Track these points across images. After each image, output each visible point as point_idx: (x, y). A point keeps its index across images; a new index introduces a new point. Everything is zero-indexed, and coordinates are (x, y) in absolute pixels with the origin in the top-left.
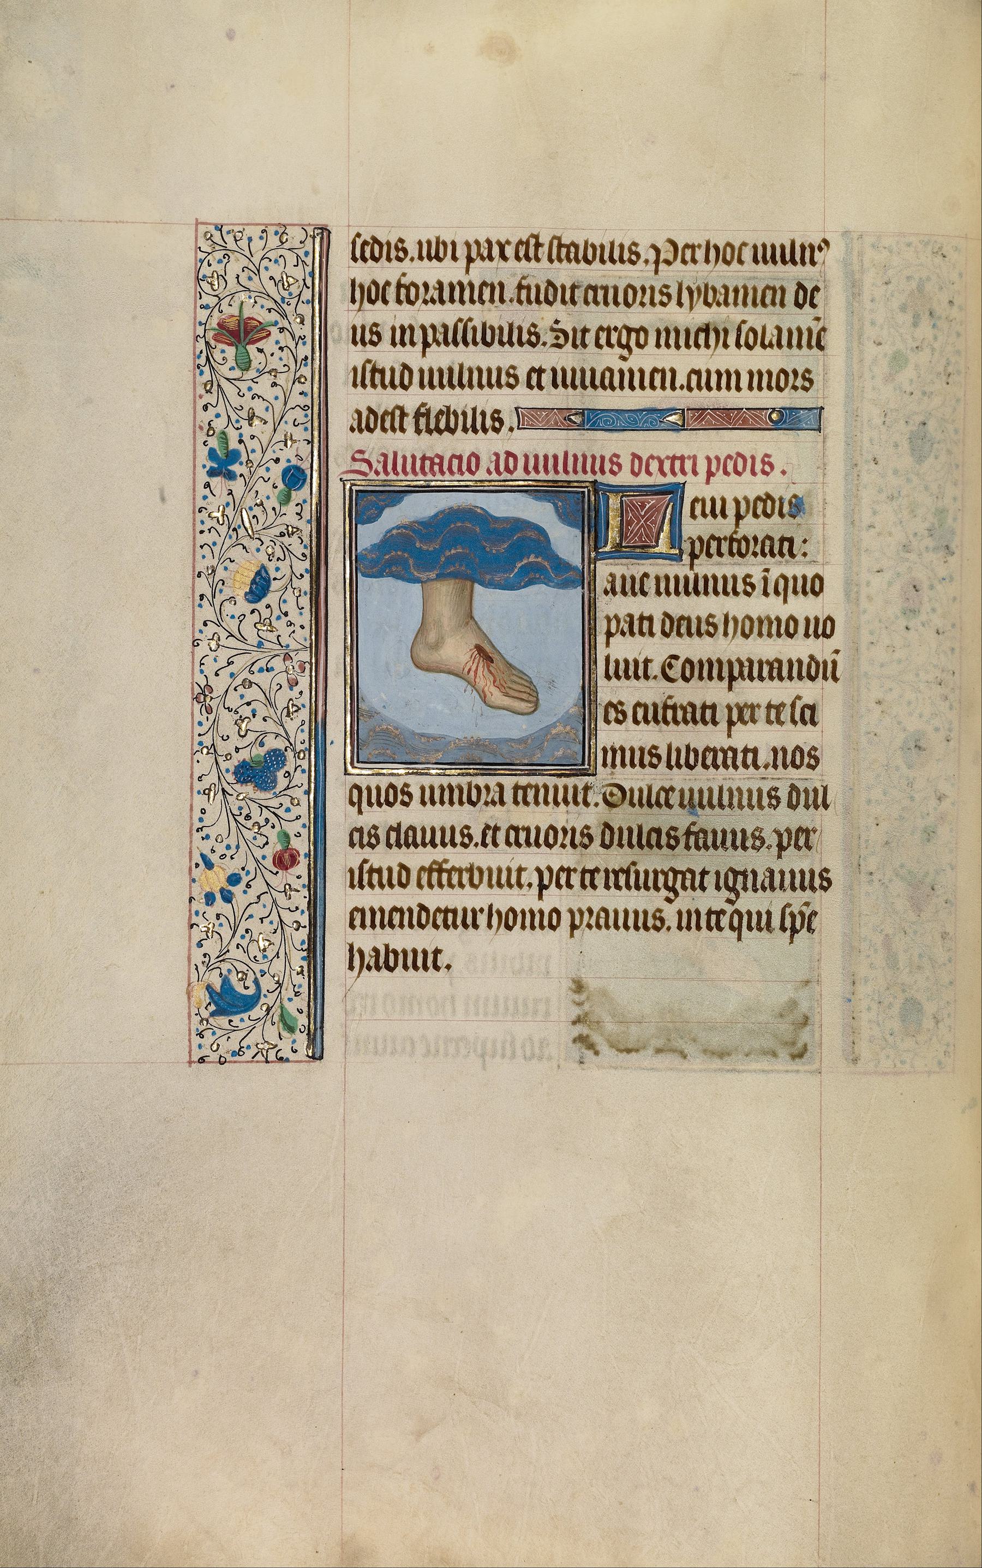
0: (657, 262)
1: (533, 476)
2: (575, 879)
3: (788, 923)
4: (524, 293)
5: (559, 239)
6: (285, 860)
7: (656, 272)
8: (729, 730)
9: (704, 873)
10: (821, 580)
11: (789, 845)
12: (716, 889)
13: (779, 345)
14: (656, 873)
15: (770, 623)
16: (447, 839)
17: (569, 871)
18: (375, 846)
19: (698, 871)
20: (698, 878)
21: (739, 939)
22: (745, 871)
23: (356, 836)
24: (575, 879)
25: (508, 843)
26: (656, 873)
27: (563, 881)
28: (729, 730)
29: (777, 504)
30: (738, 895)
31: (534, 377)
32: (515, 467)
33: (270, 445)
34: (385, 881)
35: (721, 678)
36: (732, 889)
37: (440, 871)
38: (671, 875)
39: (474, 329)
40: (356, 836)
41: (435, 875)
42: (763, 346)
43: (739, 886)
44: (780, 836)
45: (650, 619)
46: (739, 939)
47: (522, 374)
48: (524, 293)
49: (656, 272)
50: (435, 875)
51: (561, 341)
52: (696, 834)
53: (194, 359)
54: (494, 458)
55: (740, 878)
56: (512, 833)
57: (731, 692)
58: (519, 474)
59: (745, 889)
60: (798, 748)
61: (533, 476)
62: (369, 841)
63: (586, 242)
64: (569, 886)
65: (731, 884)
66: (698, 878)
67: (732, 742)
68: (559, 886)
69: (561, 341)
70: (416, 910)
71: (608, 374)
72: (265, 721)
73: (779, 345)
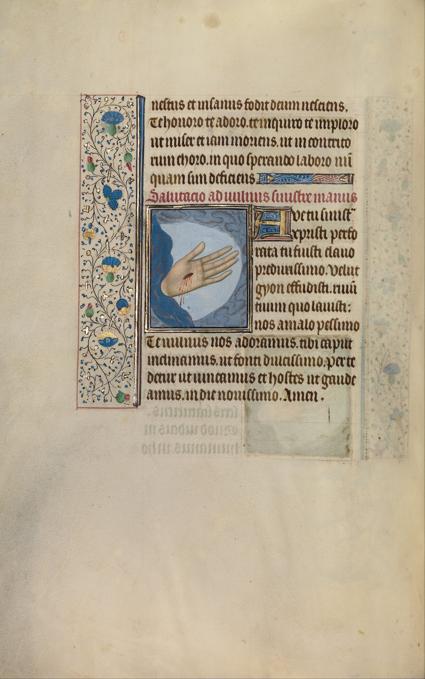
1: (228, 202)
2: (345, 362)
9: (214, 392)
10: (353, 250)
15: (325, 122)
16: (197, 344)
17: (341, 359)
24: (345, 362)
27: (339, 363)
30: (327, 386)
31: (200, 141)
32: (221, 199)
33: (94, 142)
34: (166, 379)
37: (297, 286)
41: (294, 288)
43: (328, 382)
45: (259, 358)
47: (256, 376)
50: (294, 288)
51: (155, 199)
53: (81, 136)
56: (324, 342)
57: (313, 301)
58: (223, 202)
60: (265, 321)
61: (228, 202)
63: (168, 193)
64: (342, 365)
65: (324, 382)
68: (337, 365)
69: (155, 199)
71: (183, 359)
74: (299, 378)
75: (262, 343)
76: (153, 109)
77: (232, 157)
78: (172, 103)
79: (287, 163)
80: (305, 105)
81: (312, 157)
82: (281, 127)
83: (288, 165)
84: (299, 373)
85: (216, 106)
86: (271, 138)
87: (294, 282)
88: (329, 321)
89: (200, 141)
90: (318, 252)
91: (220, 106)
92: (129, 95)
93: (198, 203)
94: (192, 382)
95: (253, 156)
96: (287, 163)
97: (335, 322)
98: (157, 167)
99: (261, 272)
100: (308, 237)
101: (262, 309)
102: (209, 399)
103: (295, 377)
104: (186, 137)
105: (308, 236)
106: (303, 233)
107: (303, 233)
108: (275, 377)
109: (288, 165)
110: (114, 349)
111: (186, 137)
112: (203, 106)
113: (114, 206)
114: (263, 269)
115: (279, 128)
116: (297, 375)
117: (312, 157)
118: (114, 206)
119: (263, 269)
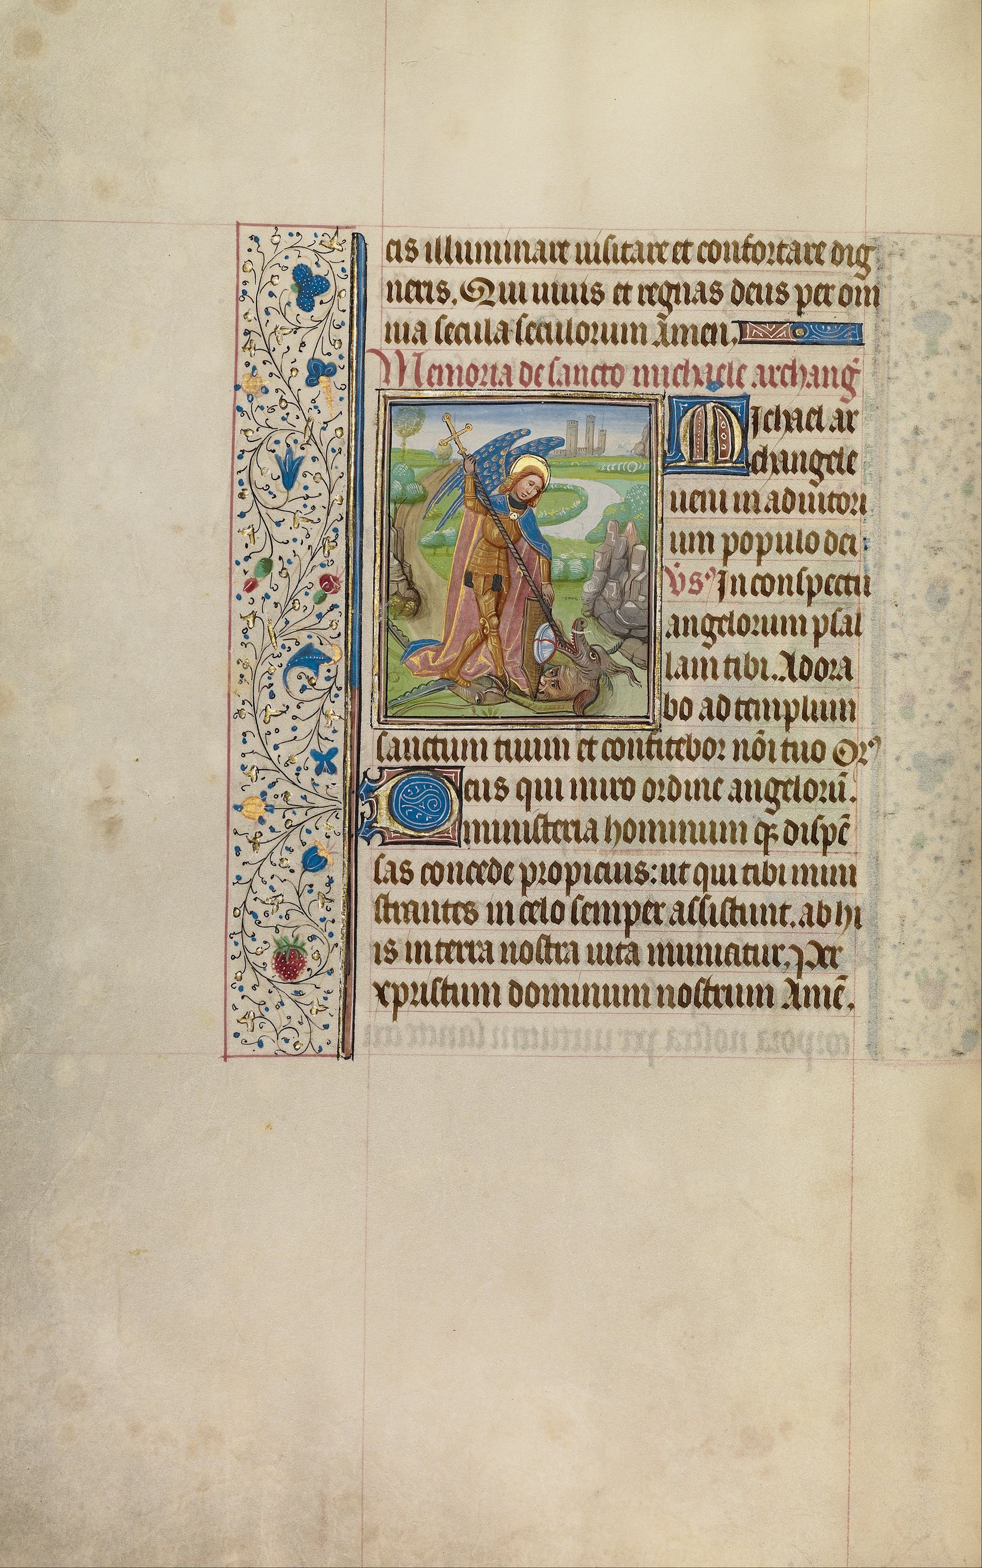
3: (805, 587)
5: (733, 901)
8: (395, 1011)
12: (427, 260)
13: (685, 675)
14: (613, 782)
18: (414, 259)
19: (778, 906)
23: (393, 249)
25: (605, 757)
26: (613, 782)
28: (395, 1011)
36: (817, 472)
38: (665, 290)
40: (393, 249)
42: (834, 633)
52: (754, 247)
54: (706, 704)
59: (677, 301)
62: (593, 298)
65: (771, 795)
72: (238, 663)
73: (685, 675)
76: (390, 299)
77: (714, 868)
78: (454, 987)
84: (787, 237)
85: (771, 506)
86: (492, 780)
91: (821, 380)
92: (229, 668)
93: (588, 389)
94: (572, 263)
95: (827, 824)
97: (702, 905)
98: (605, 899)
101: (708, 505)
102: (513, 945)
104: (525, 322)
105: (541, 878)
108: (674, 702)
111: (525, 322)
112: (626, 995)
113: (306, 303)
118: (306, 303)
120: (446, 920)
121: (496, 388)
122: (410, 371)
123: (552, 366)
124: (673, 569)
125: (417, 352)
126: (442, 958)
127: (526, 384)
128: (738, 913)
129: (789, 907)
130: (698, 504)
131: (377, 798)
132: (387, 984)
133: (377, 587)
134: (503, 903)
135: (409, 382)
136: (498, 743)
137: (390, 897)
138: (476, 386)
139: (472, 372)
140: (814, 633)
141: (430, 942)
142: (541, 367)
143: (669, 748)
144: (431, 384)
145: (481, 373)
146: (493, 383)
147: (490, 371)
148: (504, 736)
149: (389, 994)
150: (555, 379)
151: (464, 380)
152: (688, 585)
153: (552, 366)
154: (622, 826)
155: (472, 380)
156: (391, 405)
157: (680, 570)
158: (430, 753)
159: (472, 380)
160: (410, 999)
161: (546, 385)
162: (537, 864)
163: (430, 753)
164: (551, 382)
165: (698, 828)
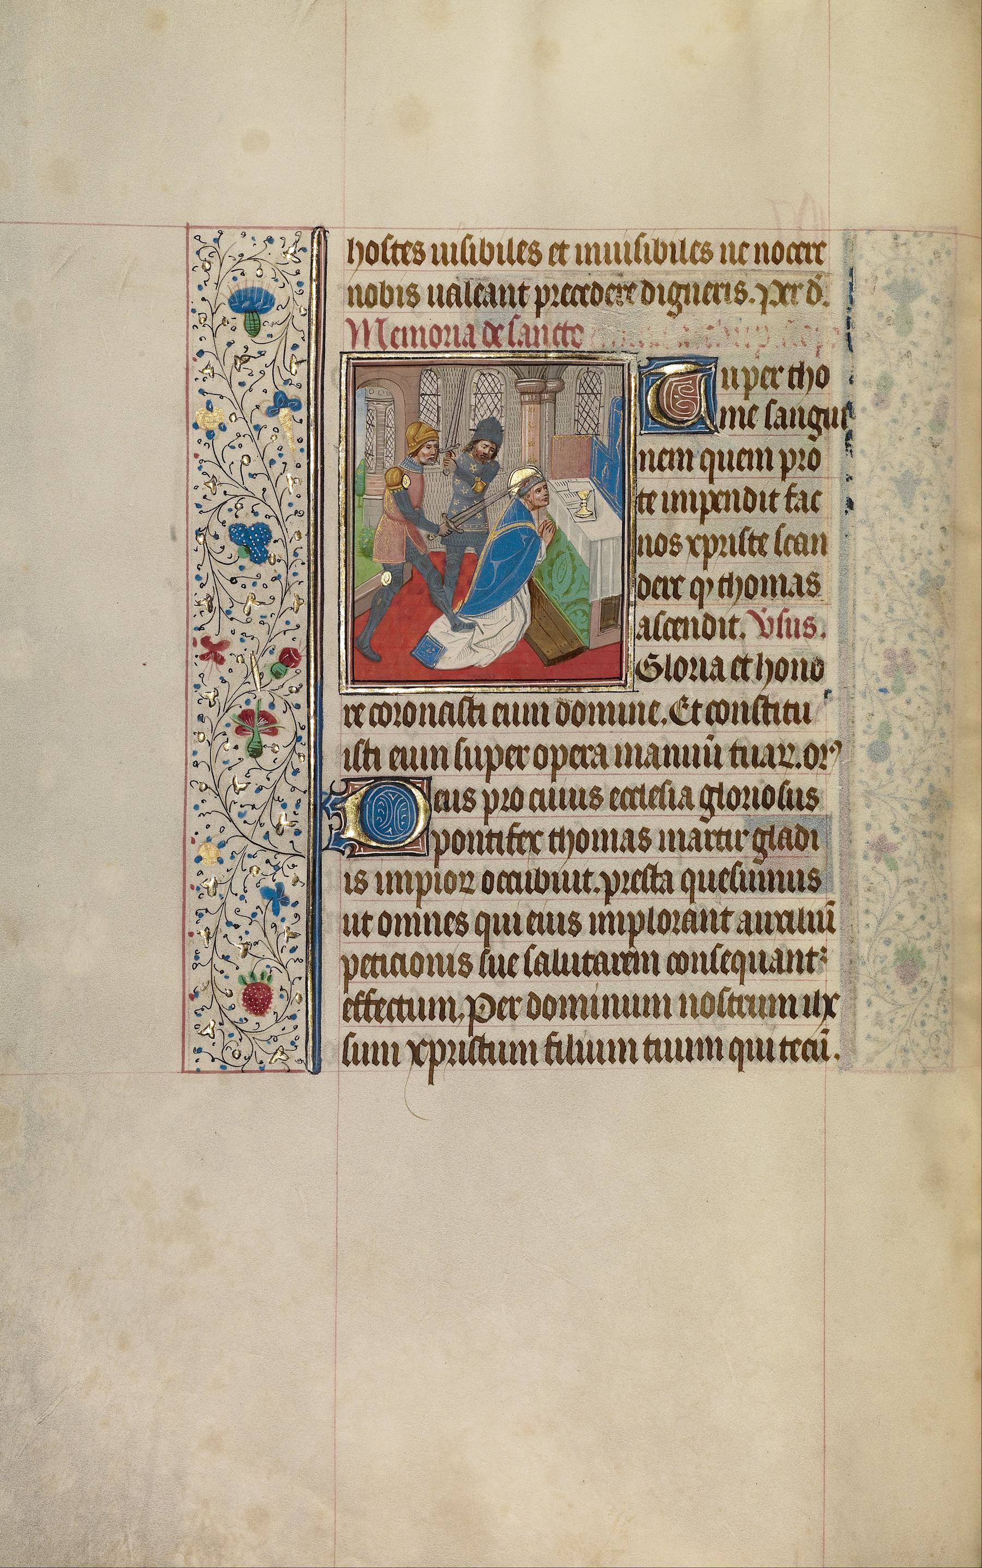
0: (763, 303)
4: (554, 1050)
6: (288, 658)
7: (764, 312)
11: (564, 763)
20: (517, 294)
21: (740, 1069)
22: (686, 618)
29: (759, 499)
30: (680, 309)
35: (694, 509)
39: (473, 247)
44: (472, 1002)
46: (740, 1069)
48: (554, 1050)
49: (764, 312)
55: (683, 292)
66: (517, 294)
67: (696, 908)
70: (742, 493)
74: (415, 251)
75: (685, 921)
79: (722, 706)
80: (762, 250)
81: (734, 1061)
82: (721, 468)
83: (716, 493)
87: (361, 993)
88: (730, 869)
89: (557, 254)
90: (372, 758)
96: (722, 706)
99: (547, 300)
100: (452, 1062)
103: (403, 247)
105: (692, 675)
106: (711, 543)
107: (711, 543)
109: (716, 493)
110: (264, 490)
114: (552, 293)
115: (716, 470)
116: (408, 244)
117: (734, 1061)
119: (552, 293)
120: (490, 850)
121: (460, 349)
122: (373, 337)
123: (511, 324)
124: (761, 614)
125: (381, 318)
126: (359, 930)
127: (488, 344)
128: (486, 1051)
129: (738, 620)
130: (745, 463)
131: (343, 809)
132: (423, 1043)
133: (343, 548)
134: (777, 575)
135: (374, 346)
136: (497, 706)
137: (486, 1037)
138: (442, 347)
139: (435, 332)
140: (782, 467)
141: (645, 1062)
142: (501, 327)
143: (510, 842)
144: (394, 344)
145: (444, 333)
146: (457, 344)
147: (452, 332)
148: (502, 699)
149: (425, 1052)
150: (460, 340)
151: (427, 342)
152: (669, 547)
153: (511, 324)
154: (576, 835)
155: (436, 340)
156: (355, 366)
157: (767, 614)
158: (559, 339)
159: (436, 340)
160: (500, 805)
161: (505, 346)
162: (797, 451)
163: (559, 339)
164: (511, 343)
165: (682, 752)
